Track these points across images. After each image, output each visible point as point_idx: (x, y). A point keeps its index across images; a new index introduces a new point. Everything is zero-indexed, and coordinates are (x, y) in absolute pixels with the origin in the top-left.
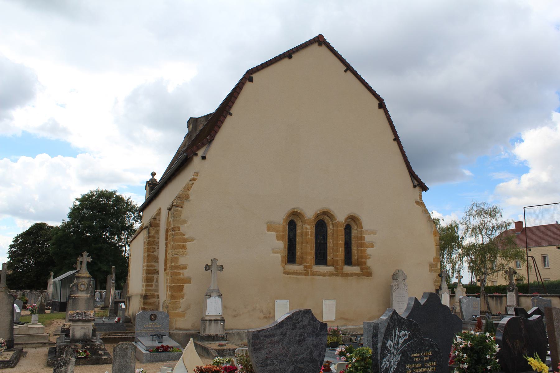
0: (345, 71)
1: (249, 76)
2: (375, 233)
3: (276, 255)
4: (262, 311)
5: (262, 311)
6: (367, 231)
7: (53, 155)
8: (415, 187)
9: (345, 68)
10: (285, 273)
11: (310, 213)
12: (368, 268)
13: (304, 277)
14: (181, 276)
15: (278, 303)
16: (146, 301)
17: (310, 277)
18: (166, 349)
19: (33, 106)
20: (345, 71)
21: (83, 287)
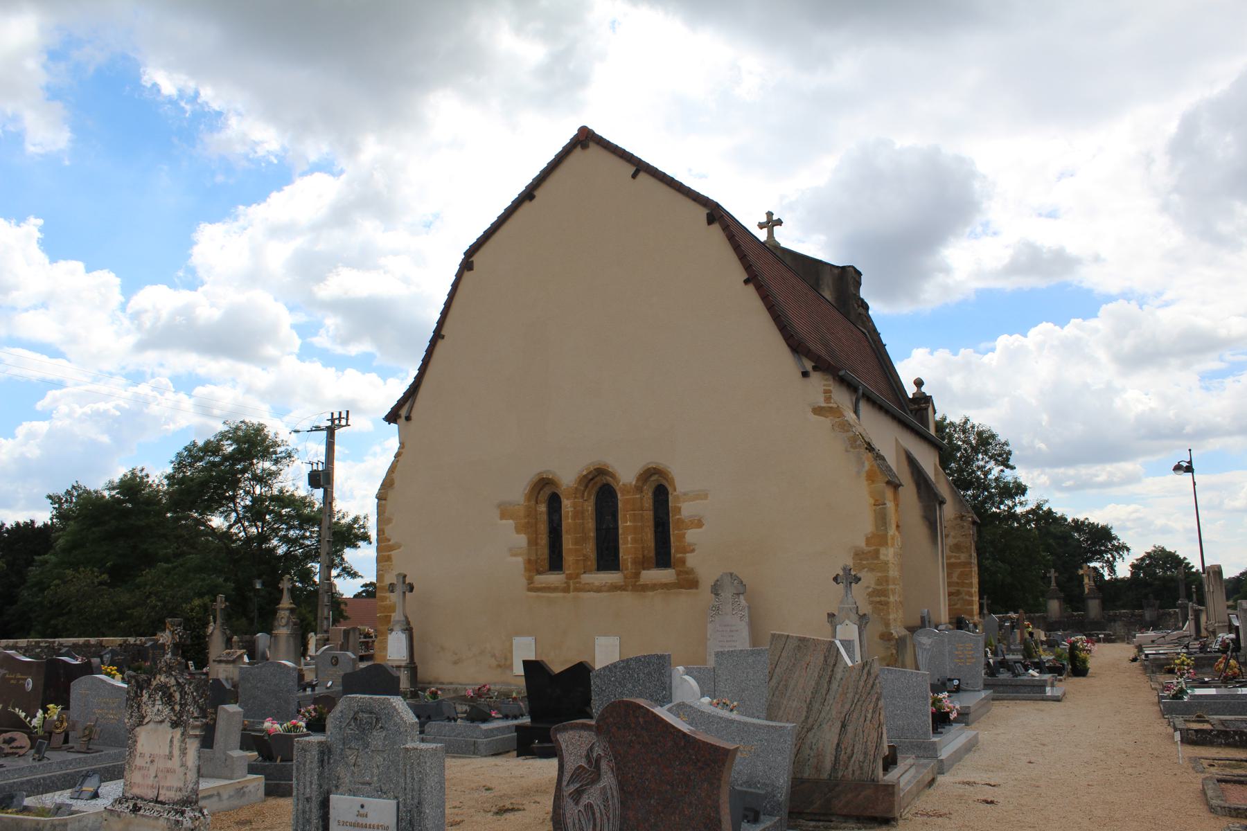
0: (634, 176)
1: (467, 264)
2: (706, 497)
3: (514, 559)
4: (494, 656)
5: (494, 656)
6: (685, 494)
7: (1061, 322)
8: (805, 374)
9: (632, 169)
10: (530, 590)
11: (568, 476)
12: (691, 571)
13: (561, 594)
14: (388, 602)
15: (517, 641)
16: (326, 635)
17: (572, 594)
18: (171, 696)
19: (995, 234)
20: (634, 176)
21: (284, 621)
